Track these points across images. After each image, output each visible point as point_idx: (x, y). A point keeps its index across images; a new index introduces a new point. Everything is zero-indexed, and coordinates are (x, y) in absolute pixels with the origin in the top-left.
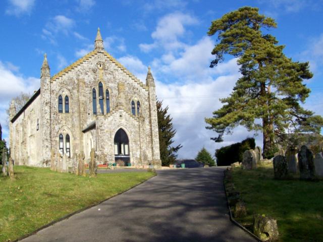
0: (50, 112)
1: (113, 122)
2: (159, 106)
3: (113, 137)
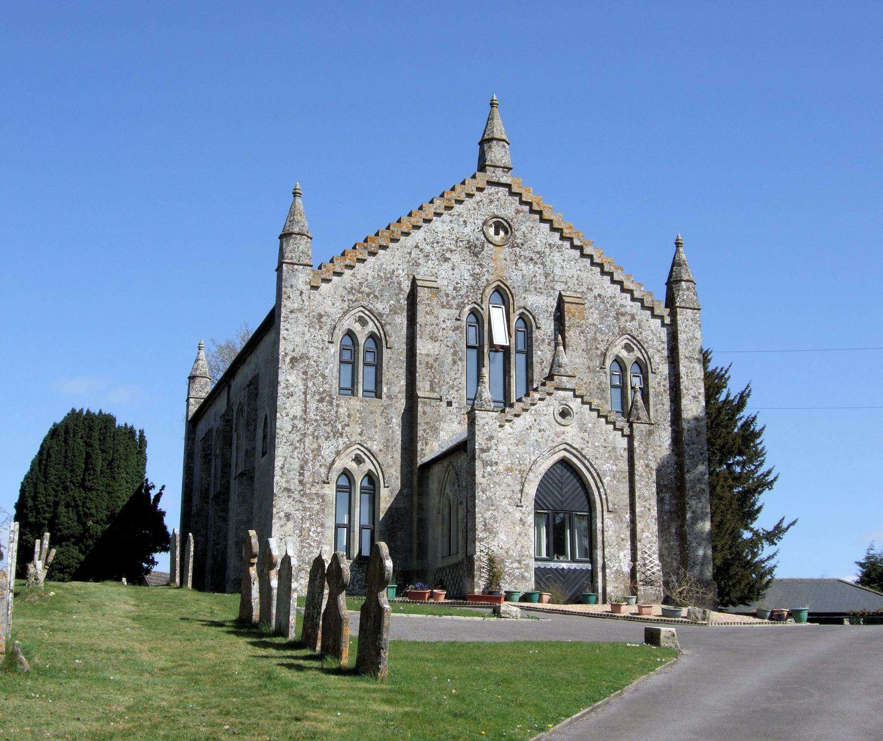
0: (305, 393)
1: (534, 435)
2: (705, 359)
3: (532, 490)
